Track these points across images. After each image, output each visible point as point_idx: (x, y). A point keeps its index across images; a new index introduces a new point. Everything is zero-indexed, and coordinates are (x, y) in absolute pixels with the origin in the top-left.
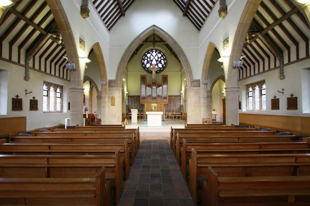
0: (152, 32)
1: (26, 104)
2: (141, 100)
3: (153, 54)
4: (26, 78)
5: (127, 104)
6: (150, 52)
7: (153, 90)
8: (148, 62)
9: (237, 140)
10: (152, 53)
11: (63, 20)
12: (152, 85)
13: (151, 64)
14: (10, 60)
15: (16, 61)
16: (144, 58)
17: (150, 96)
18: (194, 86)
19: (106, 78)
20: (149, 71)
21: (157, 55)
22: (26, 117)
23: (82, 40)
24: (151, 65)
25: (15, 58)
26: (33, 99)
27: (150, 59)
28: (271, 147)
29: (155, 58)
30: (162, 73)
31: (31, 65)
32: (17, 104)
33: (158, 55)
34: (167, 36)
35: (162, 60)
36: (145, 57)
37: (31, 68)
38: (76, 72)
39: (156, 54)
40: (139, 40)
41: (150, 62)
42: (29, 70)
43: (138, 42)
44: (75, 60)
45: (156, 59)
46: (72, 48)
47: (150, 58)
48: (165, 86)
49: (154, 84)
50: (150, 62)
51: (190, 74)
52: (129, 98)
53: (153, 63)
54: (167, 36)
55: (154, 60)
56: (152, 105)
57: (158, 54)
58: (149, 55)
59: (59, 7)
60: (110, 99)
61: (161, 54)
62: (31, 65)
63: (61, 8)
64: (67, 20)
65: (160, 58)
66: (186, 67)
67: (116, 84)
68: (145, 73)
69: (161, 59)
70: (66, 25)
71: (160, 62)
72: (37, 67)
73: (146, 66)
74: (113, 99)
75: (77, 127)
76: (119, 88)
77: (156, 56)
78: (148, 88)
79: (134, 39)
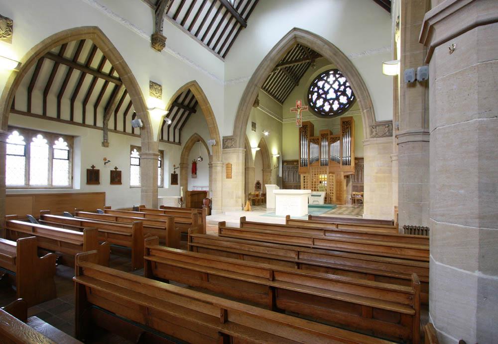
0: (292, 42)
1: (105, 177)
2: (299, 167)
3: (328, 80)
4: (105, 143)
5: (281, 175)
6: (324, 77)
7: (322, 149)
8: (319, 97)
9: (293, 255)
10: (327, 78)
11: (118, 62)
12: (320, 139)
13: (325, 100)
14: (83, 124)
15: (92, 123)
16: (311, 90)
17: (317, 160)
18: (377, 136)
19: (216, 135)
20: (320, 112)
21: (337, 79)
22: (105, 193)
23: (153, 83)
24: (324, 102)
25: (90, 120)
26: (115, 170)
27: (323, 90)
28: (313, 285)
29: (333, 86)
30: (346, 113)
31: (111, 125)
32: (93, 176)
33: (339, 79)
34: (319, 42)
35: (348, 89)
36: (313, 89)
37: (111, 131)
38: (146, 130)
39: (334, 79)
40: (269, 62)
41: (324, 96)
42: (109, 133)
43: (269, 65)
44: (142, 113)
45: (334, 89)
46: (136, 97)
47: (323, 88)
48: (347, 140)
49: (324, 136)
50: (324, 96)
51: (367, 111)
52: (285, 164)
53: (329, 97)
54: (319, 42)
55: (332, 91)
56: (320, 177)
57: (339, 77)
58: (320, 84)
59: (108, 47)
60: (225, 167)
61: (332, 74)
62: (111, 125)
63: (111, 47)
64: (124, 61)
65: (344, 84)
66: (360, 97)
67: (233, 142)
68: (313, 119)
69: (346, 87)
70: (123, 68)
71: (344, 93)
72: (120, 127)
73: (315, 103)
74: (229, 167)
75: (141, 209)
76: (237, 149)
77: (334, 82)
78: (313, 145)
79: (261, 61)
